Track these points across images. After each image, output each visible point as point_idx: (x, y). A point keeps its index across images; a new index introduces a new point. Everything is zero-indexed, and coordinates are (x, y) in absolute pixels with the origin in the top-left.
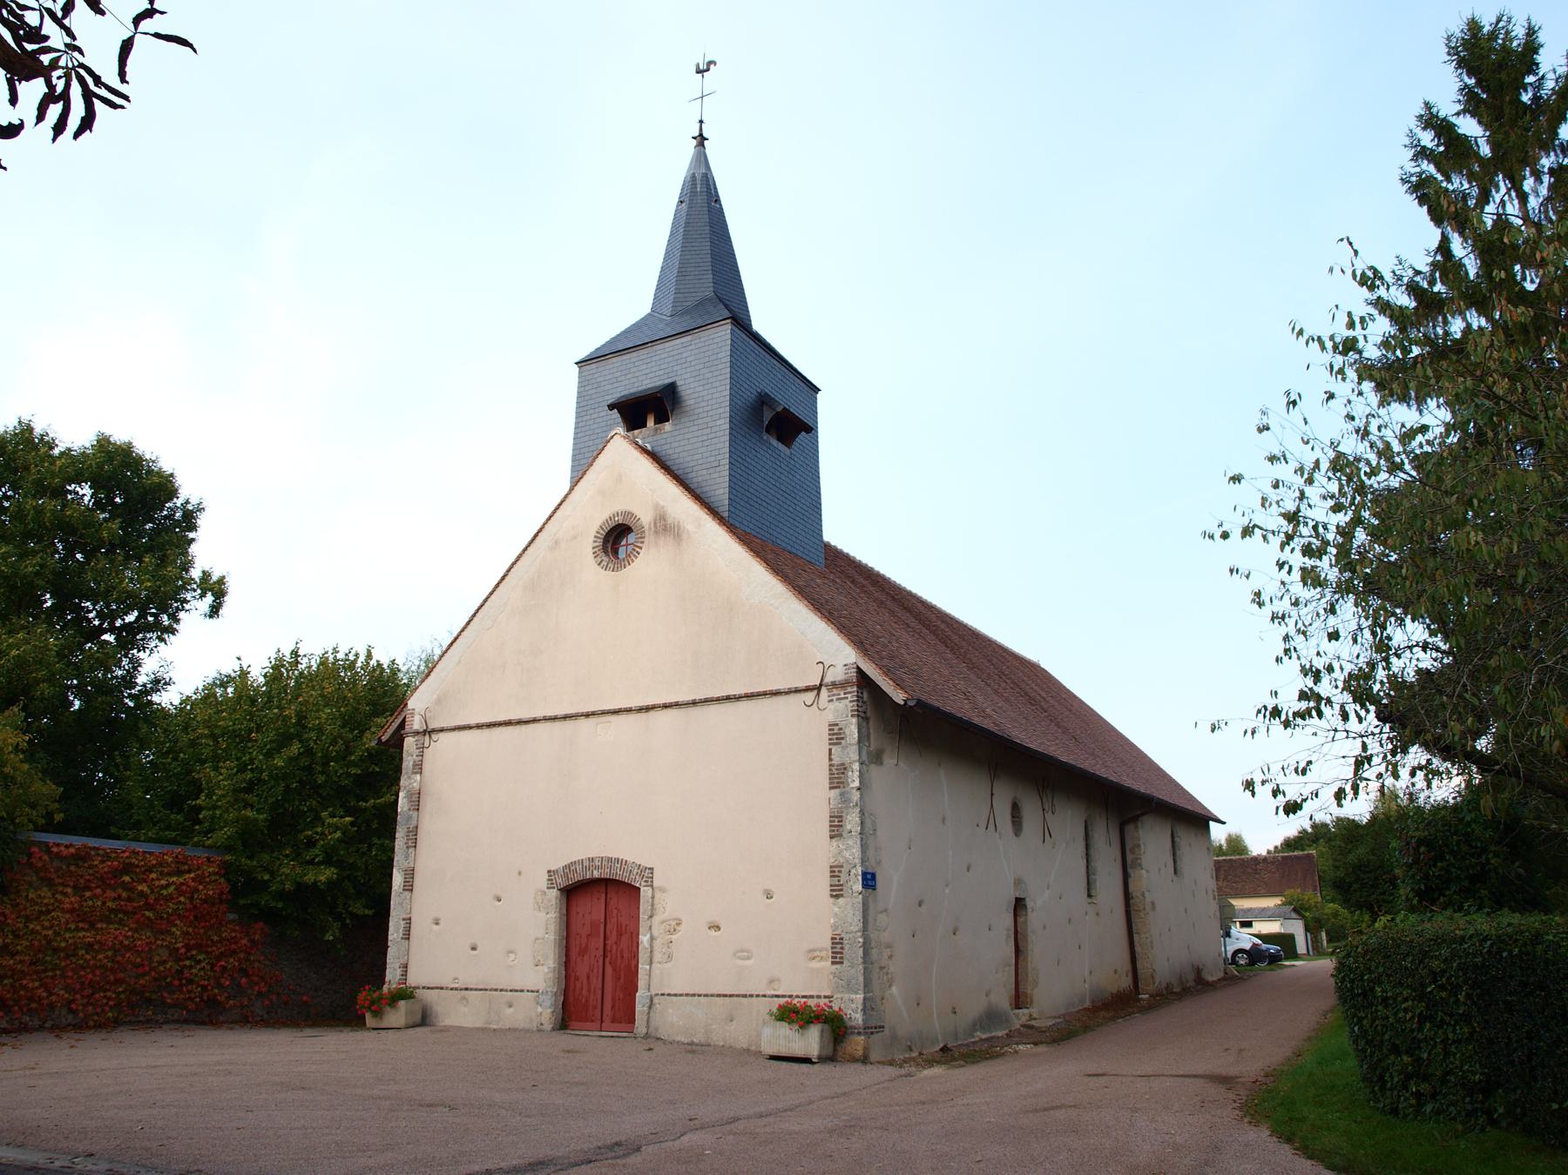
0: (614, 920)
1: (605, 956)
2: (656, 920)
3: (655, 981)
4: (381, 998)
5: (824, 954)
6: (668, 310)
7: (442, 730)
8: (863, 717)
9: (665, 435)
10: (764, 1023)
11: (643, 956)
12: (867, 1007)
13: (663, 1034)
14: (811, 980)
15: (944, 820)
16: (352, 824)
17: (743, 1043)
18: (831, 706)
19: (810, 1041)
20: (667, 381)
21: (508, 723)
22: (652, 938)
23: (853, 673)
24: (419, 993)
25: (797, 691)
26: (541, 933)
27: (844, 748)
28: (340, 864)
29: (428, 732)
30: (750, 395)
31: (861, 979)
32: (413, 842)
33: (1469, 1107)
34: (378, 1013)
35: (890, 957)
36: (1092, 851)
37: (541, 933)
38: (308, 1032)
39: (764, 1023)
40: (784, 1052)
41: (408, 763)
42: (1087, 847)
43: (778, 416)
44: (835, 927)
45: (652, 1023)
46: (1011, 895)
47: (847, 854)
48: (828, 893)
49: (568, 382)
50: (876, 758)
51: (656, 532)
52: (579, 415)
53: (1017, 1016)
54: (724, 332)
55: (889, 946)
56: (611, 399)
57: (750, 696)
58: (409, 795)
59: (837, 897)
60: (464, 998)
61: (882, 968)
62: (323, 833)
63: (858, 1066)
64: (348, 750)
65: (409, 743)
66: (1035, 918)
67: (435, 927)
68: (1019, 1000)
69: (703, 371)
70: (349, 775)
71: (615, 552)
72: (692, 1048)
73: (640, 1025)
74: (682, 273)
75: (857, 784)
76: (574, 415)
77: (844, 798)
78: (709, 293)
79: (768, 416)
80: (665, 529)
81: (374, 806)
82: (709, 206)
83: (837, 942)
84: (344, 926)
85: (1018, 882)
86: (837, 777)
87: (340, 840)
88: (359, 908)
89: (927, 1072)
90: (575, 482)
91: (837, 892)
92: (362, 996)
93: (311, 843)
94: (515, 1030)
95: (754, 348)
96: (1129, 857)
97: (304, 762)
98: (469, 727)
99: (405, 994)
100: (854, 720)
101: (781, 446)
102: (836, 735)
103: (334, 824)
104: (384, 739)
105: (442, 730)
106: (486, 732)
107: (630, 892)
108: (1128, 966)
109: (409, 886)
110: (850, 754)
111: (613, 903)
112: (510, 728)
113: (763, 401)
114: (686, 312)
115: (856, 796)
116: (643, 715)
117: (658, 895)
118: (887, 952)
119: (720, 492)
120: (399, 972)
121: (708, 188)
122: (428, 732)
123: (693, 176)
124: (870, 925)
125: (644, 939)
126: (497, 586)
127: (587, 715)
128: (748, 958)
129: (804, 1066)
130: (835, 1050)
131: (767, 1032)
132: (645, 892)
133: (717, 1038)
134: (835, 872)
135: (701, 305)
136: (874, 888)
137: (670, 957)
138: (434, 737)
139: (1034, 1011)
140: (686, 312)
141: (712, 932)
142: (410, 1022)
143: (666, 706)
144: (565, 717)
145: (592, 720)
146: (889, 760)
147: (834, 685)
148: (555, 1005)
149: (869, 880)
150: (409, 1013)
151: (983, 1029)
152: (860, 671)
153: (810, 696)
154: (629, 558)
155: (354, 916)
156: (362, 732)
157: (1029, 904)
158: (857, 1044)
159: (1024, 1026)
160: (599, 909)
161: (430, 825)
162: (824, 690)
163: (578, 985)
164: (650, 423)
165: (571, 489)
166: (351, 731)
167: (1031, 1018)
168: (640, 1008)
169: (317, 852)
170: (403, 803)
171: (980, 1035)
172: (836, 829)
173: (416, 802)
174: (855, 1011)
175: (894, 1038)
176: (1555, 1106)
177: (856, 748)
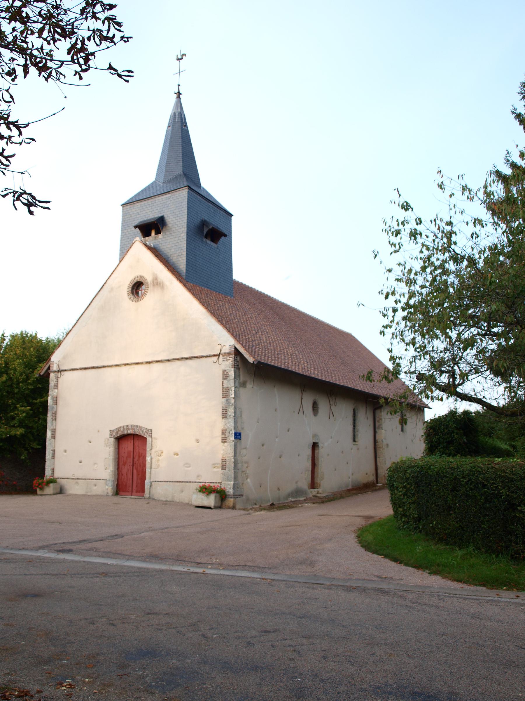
0: (137, 451)
1: (133, 466)
2: (153, 451)
3: (152, 475)
4: (43, 482)
5: (219, 465)
6: (162, 180)
7: (65, 370)
8: (237, 368)
10: (194, 493)
11: (148, 466)
12: (235, 487)
13: (156, 497)
14: (214, 477)
15: (276, 410)
16: (31, 410)
17: (186, 501)
18: (224, 363)
19: (211, 500)
20: (160, 215)
21: (93, 368)
22: (151, 459)
23: (233, 349)
24: (58, 480)
25: (210, 356)
27: (229, 381)
28: (27, 427)
29: (60, 371)
30: (197, 221)
31: (233, 476)
32: (55, 418)
33: (415, 526)
34: (42, 489)
35: (247, 467)
36: (357, 422)
38: (15, 496)
39: (194, 493)
40: (201, 504)
41: (52, 384)
42: (354, 420)
43: (211, 229)
44: (223, 455)
45: (152, 493)
46: (311, 441)
47: (228, 425)
49: (117, 216)
50: (243, 385)
51: (154, 285)
52: (123, 230)
53: (311, 492)
54: (184, 193)
55: (246, 462)
56: (136, 223)
57: (191, 358)
58: (53, 398)
59: (224, 442)
60: (77, 483)
61: (243, 471)
62: (18, 414)
63: (230, 510)
64: (28, 378)
65: (52, 376)
66: (322, 452)
68: (313, 485)
69: (176, 209)
70: (28, 389)
71: (137, 293)
72: (166, 503)
73: (147, 494)
74: (168, 163)
75: (233, 396)
76: (120, 229)
77: (228, 402)
78: (180, 172)
79: (205, 230)
81: (40, 402)
82: (182, 127)
83: (224, 461)
84: (29, 453)
85: (315, 436)
86: (225, 394)
87: (25, 417)
88: (35, 446)
89: (257, 513)
90: (120, 262)
91: (224, 440)
92: (35, 482)
93: (13, 418)
94: (98, 495)
95: (200, 199)
96: (377, 424)
97: (9, 383)
98: (76, 369)
99: (53, 481)
100: (233, 369)
101: (212, 244)
102: (225, 376)
103: (23, 410)
104: (42, 374)
105: (65, 370)
106: (84, 371)
107: (143, 439)
108: (373, 471)
109: (54, 437)
110: (230, 383)
111: (136, 444)
113: (204, 223)
114: (170, 181)
115: (233, 401)
116: (148, 365)
118: (246, 465)
119: (182, 264)
120: (51, 472)
121: (181, 118)
122: (60, 371)
123: (175, 114)
124: (238, 455)
125: (148, 459)
126: (87, 308)
127: (125, 365)
128: (189, 467)
129: (208, 510)
130: (222, 504)
131: (195, 496)
132: (149, 440)
133: (176, 499)
134: (223, 432)
135: (176, 178)
136: (240, 439)
138: (63, 373)
139: (320, 490)
140: (170, 181)
142: (55, 492)
143: (157, 362)
144: (116, 366)
145: (127, 367)
146: (249, 386)
147: (225, 354)
148: (113, 485)
149: (238, 436)
150: (54, 489)
151: (293, 497)
152: (236, 349)
153: (215, 359)
154: (144, 294)
155: (32, 448)
156: (34, 370)
157: (320, 445)
158: (230, 502)
159: (314, 496)
160: (130, 446)
162: (221, 356)
163: (123, 477)
165: (120, 263)
166: (29, 369)
167: (318, 492)
168: (147, 487)
169: (16, 422)
170: (50, 402)
171: (291, 499)
172: (224, 415)
173: (56, 401)
174: (230, 488)
175: (248, 499)
176: (431, 525)
177: (233, 381)
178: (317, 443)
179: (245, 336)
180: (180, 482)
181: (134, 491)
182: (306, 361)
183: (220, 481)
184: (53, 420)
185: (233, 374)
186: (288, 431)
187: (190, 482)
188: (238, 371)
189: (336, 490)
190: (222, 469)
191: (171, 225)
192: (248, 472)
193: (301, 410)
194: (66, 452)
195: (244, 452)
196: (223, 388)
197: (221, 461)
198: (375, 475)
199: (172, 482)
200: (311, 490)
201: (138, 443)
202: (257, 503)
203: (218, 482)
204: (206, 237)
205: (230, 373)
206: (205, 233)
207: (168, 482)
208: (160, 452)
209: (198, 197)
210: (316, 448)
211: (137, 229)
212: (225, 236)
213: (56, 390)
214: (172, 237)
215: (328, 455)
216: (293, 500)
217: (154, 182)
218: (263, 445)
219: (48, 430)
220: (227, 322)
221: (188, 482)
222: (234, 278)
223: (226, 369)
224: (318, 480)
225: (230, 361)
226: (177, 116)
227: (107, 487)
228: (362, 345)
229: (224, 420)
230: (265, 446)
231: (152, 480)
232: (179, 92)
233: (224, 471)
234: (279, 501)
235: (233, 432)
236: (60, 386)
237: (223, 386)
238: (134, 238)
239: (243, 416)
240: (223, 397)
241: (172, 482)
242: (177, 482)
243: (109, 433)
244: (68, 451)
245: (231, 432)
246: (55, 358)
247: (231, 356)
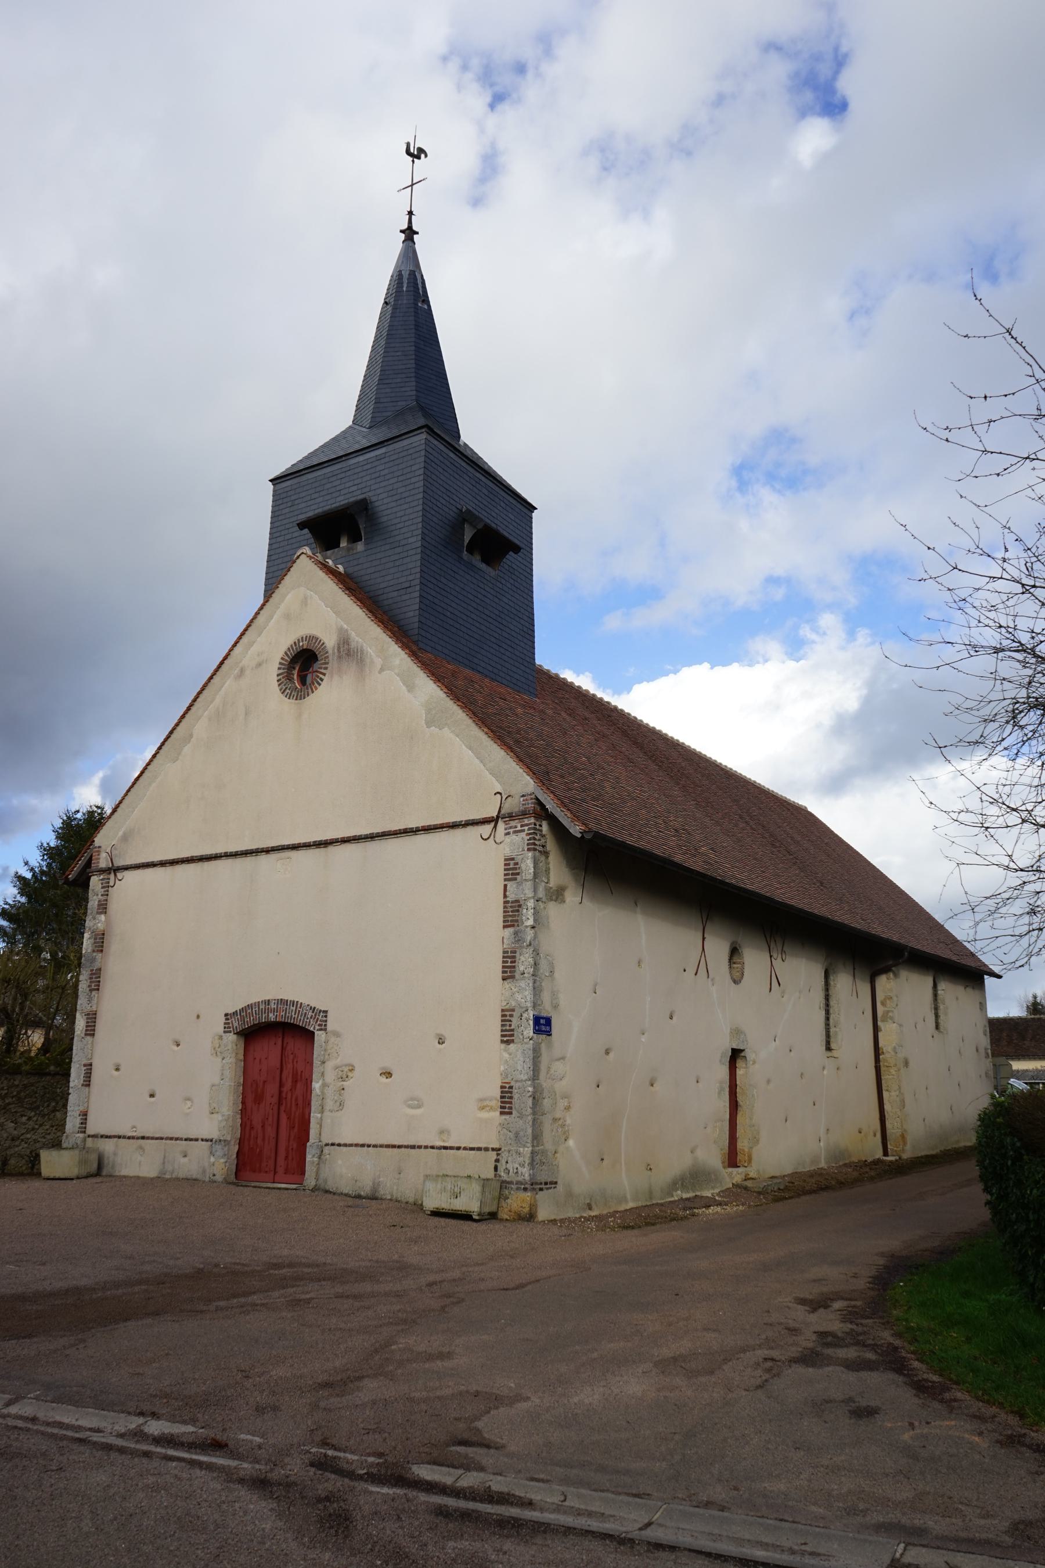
0: (290, 1066)
1: (280, 1103)
9: (349, 554)
11: (315, 1104)
13: (331, 1186)
18: (508, 839)
22: (325, 1085)
23: (531, 805)
26: (217, 1080)
29: (116, 870)
31: (530, 1131)
32: (96, 985)
35: (568, 1108)
37: (217, 1080)
41: (93, 903)
42: (827, 998)
45: (322, 1176)
46: (725, 1044)
47: (518, 997)
48: (499, 1038)
55: (565, 1096)
57: (427, 829)
59: (508, 1042)
60: (141, 1147)
61: (555, 1120)
65: (95, 881)
67: (116, 1073)
68: (732, 1159)
73: (310, 1180)
75: (531, 922)
77: (518, 937)
79: (468, 535)
80: (349, 654)
83: (506, 1094)
85: (737, 1032)
91: (508, 1037)
101: (483, 566)
102: (512, 870)
106: (169, 869)
107: (309, 1036)
109: (91, 1031)
112: (192, 866)
117: (332, 1039)
118: (563, 1103)
119: (411, 610)
120: (78, 1120)
125: (316, 1086)
126: (183, 717)
128: (419, 1107)
132: (320, 1036)
134: (506, 1016)
136: (549, 1033)
137: (341, 1105)
138: (119, 875)
141: (383, 1079)
142: (84, 1173)
145: (273, 856)
147: (511, 816)
151: (684, 1188)
152: (539, 803)
153: (486, 829)
157: (749, 1054)
161: (116, 966)
164: (344, 544)
171: (678, 1195)
173: (101, 941)
175: (570, 1195)
178: (742, 1051)
179: (562, 777)
180: (394, 1146)
181: (281, 1170)
182: (712, 849)
183: (497, 1146)
184: (91, 991)
185: (532, 865)
186: (671, 1018)
187: (420, 1147)
188: (543, 858)
189: (789, 1171)
190: (502, 1113)
191: (385, 519)
192: (569, 1121)
193: (702, 966)
194: (117, 1069)
195: (558, 1067)
196: (505, 902)
197: (499, 1090)
198: (879, 1135)
199: (375, 1146)
200: (730, 1170)
201: (294, 1045)
202: (594, 1206)
203: (491, 1146)
204: (471, 549)
205: (523, 866)
206: (466, 541)
207: (363, 1146)
208: (346, 1069)
209: (452, 455)
210: (740, 1063)
211: (306, 531)
212: (517, 549)
213: (103, 917)
214: (387, 547)
215: (769, 1082)
216: (685, 1196)
217: (350, 427)
218: (607, 1052)
219: (78, 1015)
220: (517, 742)
221: (413, 1147)
222: (538, 662)
223: (514, 855)
224: (742, 1144)
225: (523, 835)
226: (405, 281)
227: (212, 1159)
228: (832, 832)
229: (507, 984)
230: (612, 1055)
231: (325, 1141)
232: (410, 227)
233: (507, 1117)
234: (651, 1198)
235: (531, 1014)
236: (113, 906)
237: (505, 896)
238: (300, 547)
239: (556, 975)
240: (505, 927)
241: (375, 1146)
242: (388, 1146)
243: (222, 1019)
244: (122, 1068)
245: (525, 1015)
246: (103, 839)
247: (526, 821)
